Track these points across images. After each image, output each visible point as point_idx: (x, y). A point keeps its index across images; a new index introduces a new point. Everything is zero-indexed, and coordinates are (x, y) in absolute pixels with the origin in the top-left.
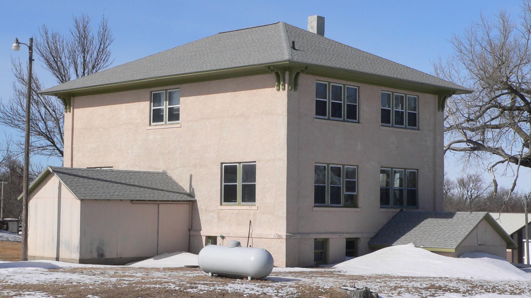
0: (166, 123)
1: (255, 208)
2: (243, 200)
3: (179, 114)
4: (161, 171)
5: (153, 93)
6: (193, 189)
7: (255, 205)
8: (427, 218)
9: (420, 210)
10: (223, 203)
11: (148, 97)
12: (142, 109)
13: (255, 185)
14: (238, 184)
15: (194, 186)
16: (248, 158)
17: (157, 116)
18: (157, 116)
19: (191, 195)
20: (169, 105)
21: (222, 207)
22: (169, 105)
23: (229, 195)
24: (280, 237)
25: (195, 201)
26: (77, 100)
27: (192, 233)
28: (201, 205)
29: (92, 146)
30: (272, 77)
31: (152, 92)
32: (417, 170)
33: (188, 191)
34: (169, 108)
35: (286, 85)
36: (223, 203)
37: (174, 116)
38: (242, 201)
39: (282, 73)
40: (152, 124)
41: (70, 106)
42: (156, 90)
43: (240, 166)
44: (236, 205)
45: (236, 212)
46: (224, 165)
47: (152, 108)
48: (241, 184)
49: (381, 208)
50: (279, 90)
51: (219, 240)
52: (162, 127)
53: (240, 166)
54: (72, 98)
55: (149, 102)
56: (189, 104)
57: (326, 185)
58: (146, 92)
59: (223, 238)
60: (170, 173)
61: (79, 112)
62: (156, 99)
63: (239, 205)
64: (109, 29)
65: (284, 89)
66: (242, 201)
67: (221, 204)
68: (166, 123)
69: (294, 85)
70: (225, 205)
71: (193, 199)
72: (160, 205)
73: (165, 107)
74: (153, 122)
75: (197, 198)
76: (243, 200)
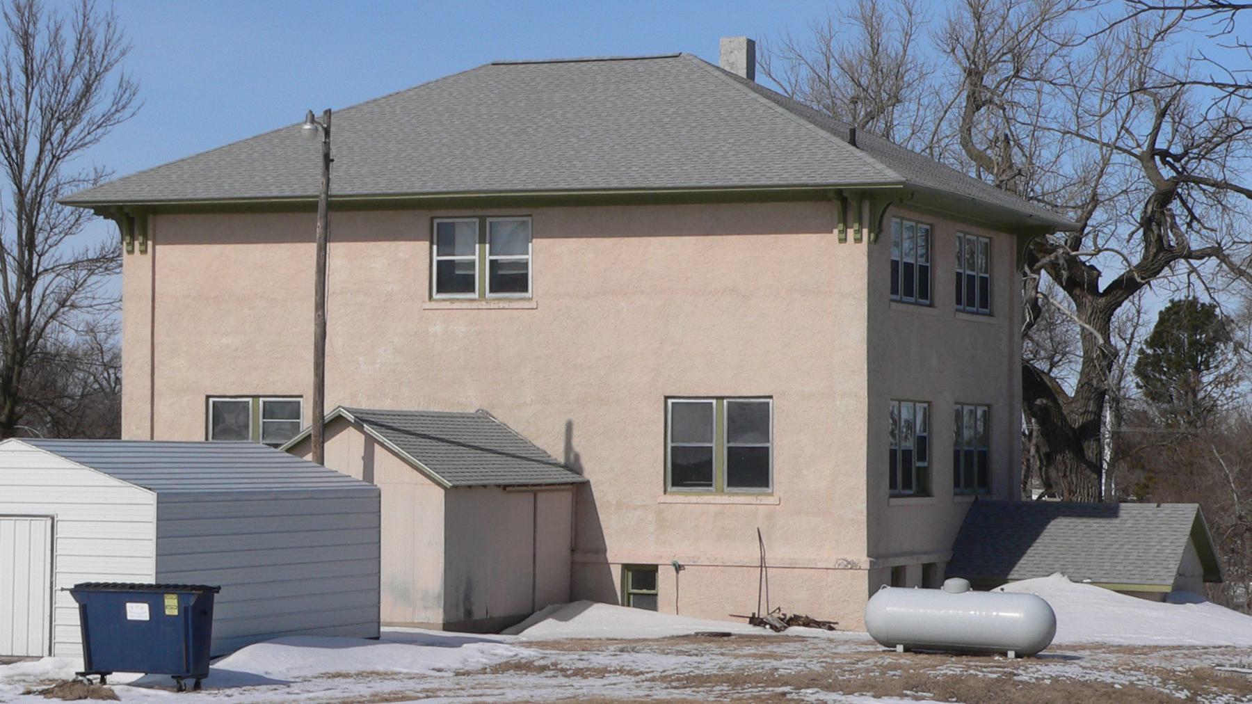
0: (482, 295)
1: (770, 500)
2: (731, 483)
3: (526, 275)
4: (472, 411)
5: (436, 221)
6: (577, 456)
7: (771, 494)
8: (1055, 517)
9: (994, 498)
10: (669, 488)
11: (426, 231)
12: (411, 258)
13: (767, 448)
14: (723, 449)
15: (577, 444)
16: (747, 387)
17: (452, 280)
18: (452, 280)
19: (573, 465)
20: (491, 254)
21: (668, 498)
22: (491, 254)
23: (688, 470)
24: (852, 566)
25: (588, 482)
26: (162, 222)
27: (579, 557)
28: (602, 493)
29: (225, 341)
30: (834, 208)
31: (432, 219)
32: (208, 397)
33: (562, 460)
34: (439, 262)
35: (865, 231)
36: (669, 488)
37: (510, 280)
38: (729, 485)
39: (845, 205)
40: (435, 296)
41: (146, 238)
42: (443, 216)
43: (720, 406)
44: (711, 493)
45: (712, 509)
46: (670, 401)
47: (435, 258)
48: (726, 445)
49: (955, 494)
50: (843, 240)
51: (665, 578)
52: (475, 305)
53: (720, 406)
54: (151, 217)
55: (427, 243)
56: (551, 258)
57: (713, 445)
58: (423, 218)
59: (678, 568)
60: (500, 416)
61: (170, 255)
62: (444, 239)
63: (722, 492)
64: (124, 43)
65: (858, 240)
66: (729, 485)
67: (665, 492)
68: (482, 295)
69: (877, 230)
70: (673, 493)
71: (577, 478)
72: (541, 496)
73: (479, 258)
74: (439, 291)
75: (588, 475)
76: (731, 483)
